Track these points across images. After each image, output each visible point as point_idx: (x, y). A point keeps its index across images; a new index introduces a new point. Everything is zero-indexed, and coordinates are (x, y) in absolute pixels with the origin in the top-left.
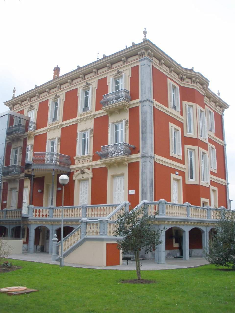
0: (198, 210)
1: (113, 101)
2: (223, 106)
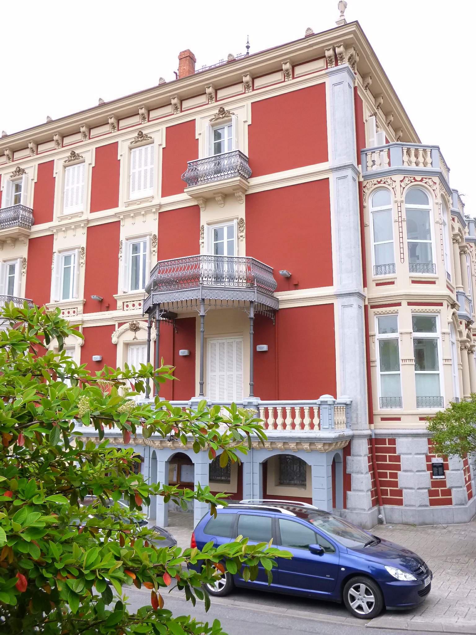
1: (223, 174)
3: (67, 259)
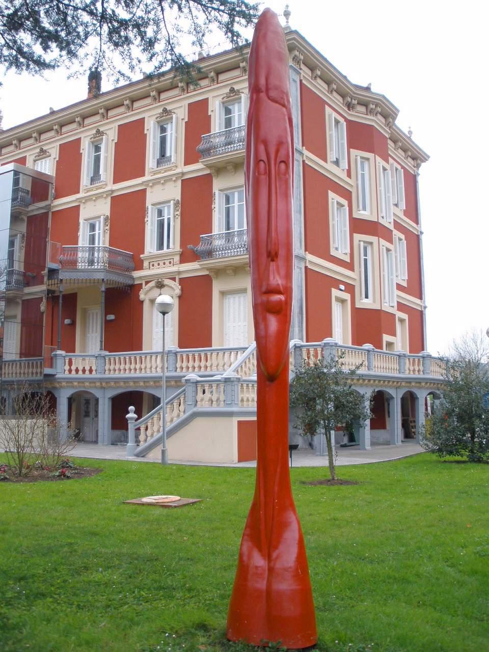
0: (383, 357)
2: (418, 157)
3: (93, 227)
